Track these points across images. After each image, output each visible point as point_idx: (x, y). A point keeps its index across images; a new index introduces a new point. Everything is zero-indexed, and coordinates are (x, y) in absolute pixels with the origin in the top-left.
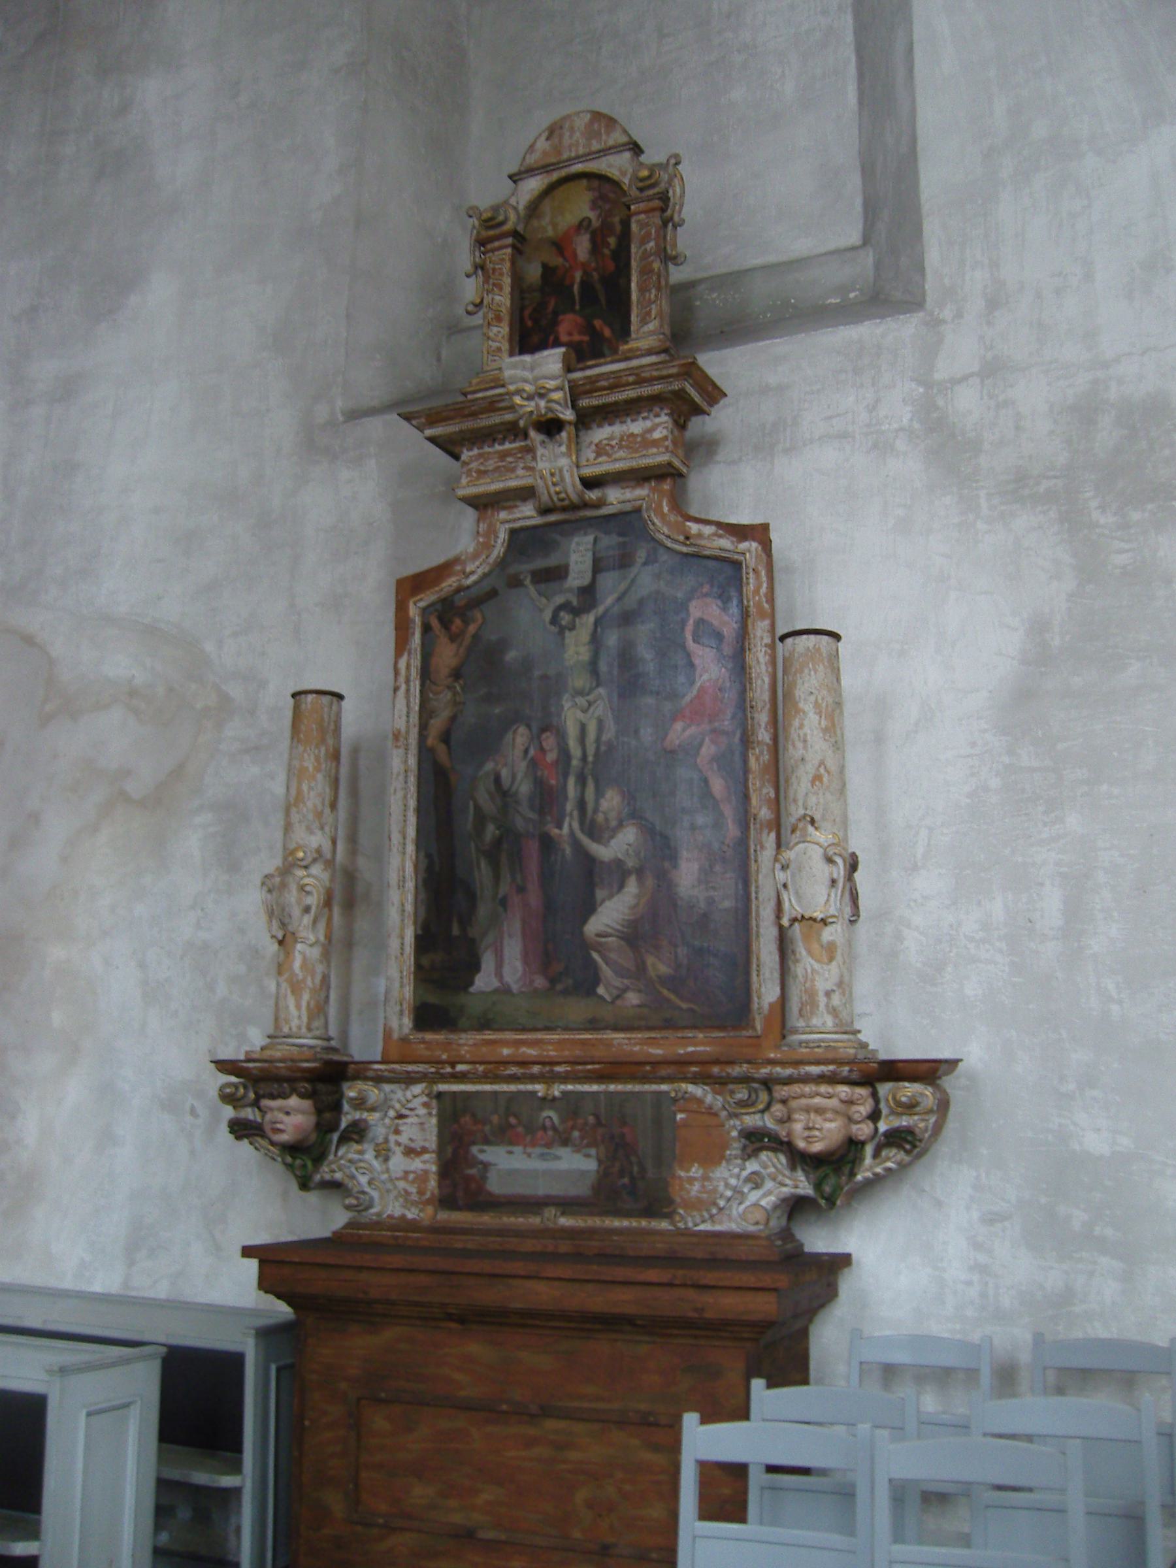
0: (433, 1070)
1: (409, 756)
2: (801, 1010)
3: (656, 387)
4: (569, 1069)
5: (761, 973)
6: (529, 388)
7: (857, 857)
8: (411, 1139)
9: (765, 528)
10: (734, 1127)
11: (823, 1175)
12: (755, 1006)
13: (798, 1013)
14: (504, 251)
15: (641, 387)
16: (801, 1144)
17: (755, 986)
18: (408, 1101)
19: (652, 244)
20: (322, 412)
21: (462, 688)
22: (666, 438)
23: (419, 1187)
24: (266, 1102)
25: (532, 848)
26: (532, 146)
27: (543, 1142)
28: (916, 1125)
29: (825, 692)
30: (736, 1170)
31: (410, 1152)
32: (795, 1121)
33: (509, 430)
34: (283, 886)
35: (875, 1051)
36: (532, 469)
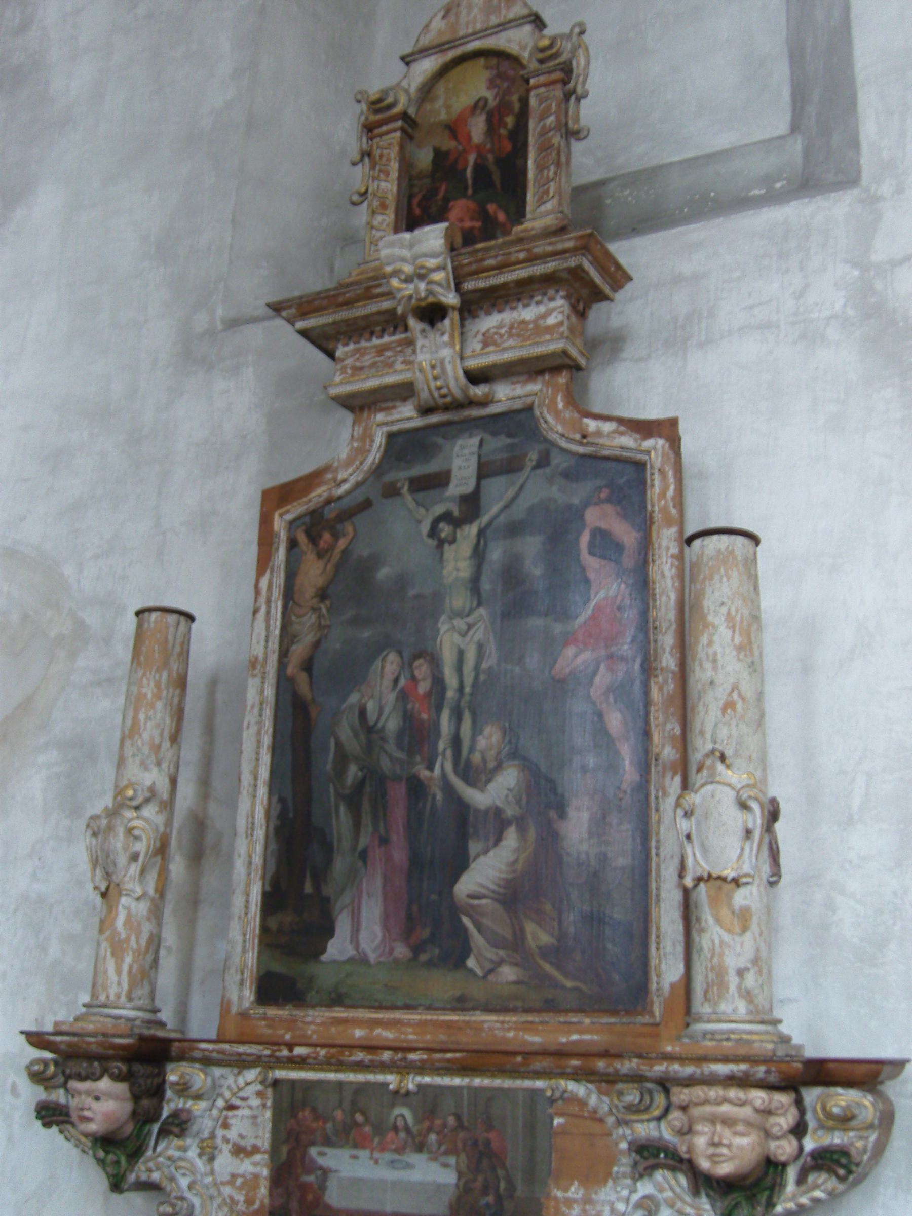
0: (267, 1052)
1: (266, 685)
2: (706, 992)
3: (550, 265)
4: (425, 1057)
5: (661, 946)
6: (408, 269)
7: (778, 804)
8: (241, 1136)
9: (673, 423)
10: (624, 1137)
11: (733, 1203)
12: (654, 986)
13: (702, 996)
14: (393, 135)
15: (534, 265)
16: (704, 1164)
17: (653, 962)
18: (240, 1089)
19: (552, 118)
20: (201, 321)
21: (328, 610)
22: (561, 324)
23: (247, 1195)
24: (74, 1084)
25: (398, 793)
26: (427, 26)
27: (393, 1147)
28: (852, 1144)
29: (740, 603)
30: (625, 1193)
31: (239, 1151)
32: (698, 1133)
33: (387, 322)
34: (110, 828)
35: (800, 1047)
36: (411, 363)
